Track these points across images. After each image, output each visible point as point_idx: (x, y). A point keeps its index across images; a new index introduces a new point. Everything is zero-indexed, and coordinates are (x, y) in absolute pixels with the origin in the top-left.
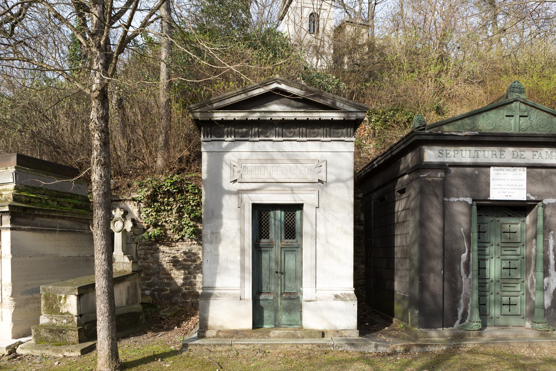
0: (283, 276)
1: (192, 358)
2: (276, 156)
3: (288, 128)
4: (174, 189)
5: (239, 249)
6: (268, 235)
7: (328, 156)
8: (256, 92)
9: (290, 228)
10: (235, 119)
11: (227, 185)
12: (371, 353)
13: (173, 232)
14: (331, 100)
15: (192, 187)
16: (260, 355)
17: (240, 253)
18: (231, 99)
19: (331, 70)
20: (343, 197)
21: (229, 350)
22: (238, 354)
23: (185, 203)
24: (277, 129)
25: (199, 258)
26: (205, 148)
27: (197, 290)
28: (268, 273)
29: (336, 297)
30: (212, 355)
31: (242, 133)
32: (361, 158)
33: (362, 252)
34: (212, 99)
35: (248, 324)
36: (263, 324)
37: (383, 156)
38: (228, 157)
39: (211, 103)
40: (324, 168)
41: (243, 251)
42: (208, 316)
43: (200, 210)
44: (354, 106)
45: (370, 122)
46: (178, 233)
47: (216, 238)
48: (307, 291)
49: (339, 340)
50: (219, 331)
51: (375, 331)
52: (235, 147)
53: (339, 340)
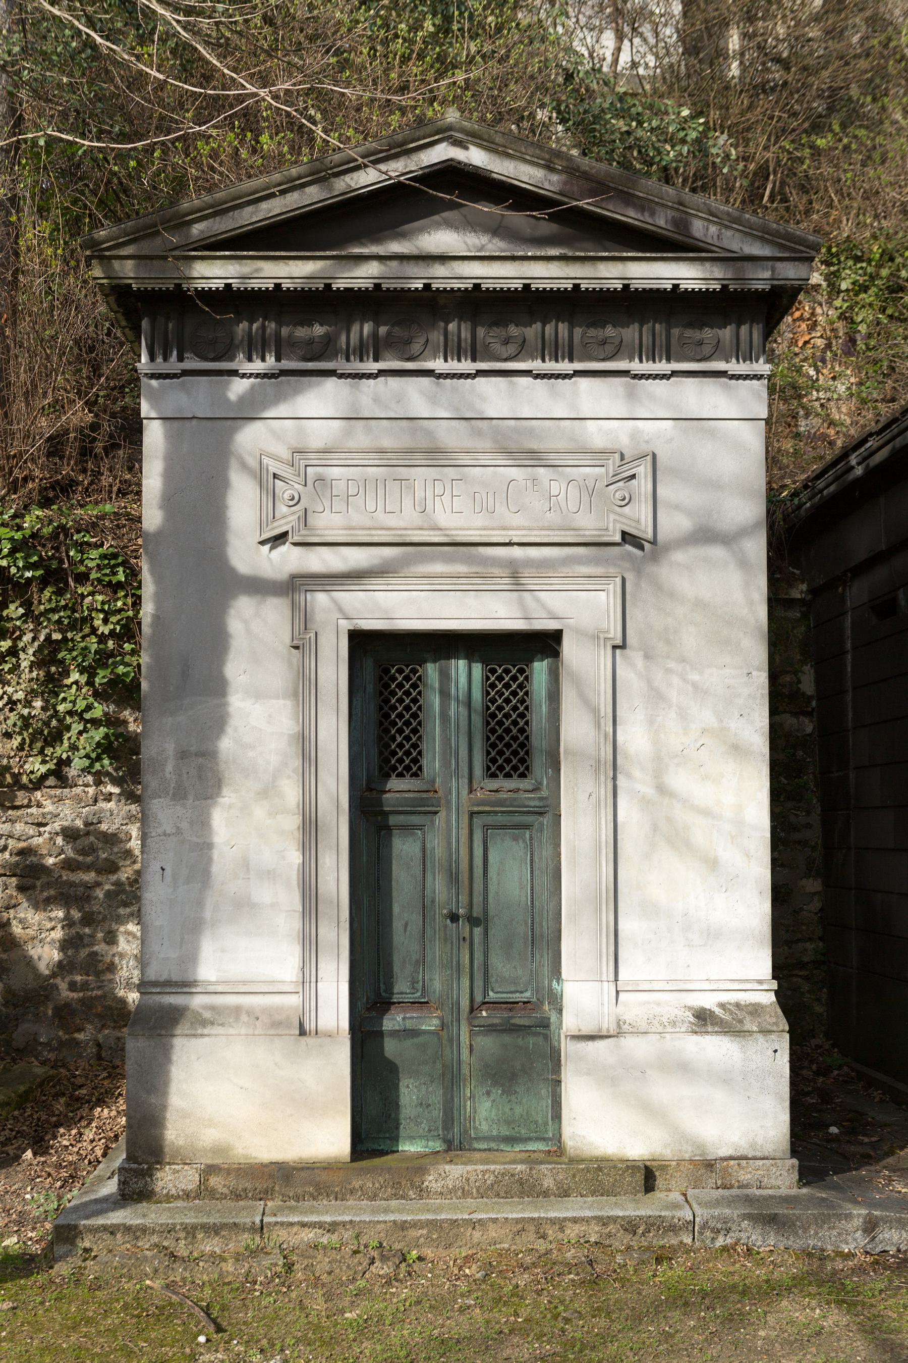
0: (478, 931)
1: (96, 1286)
2: (450, 435)
3: (496, 324)
4: (27, 567)
5: (297, 821)
6: (415, 761)
7: (658, 433)
8: (367, 178)
9: (508, 731)
10: (278, 286)
11: (246, 554)
12: (850, 1255)
13: (21, 748)
14: (670, 214)
15: (103, 557)
16: (382, 1269)
17: (298, 835)
18: (264, 205)
19: (672, 82)
20: (724, 601)
21: (255, 1253)
22: (289, 1267)
23: (72, 626)
24: (452, 326)
25: (129, 853)
26: (155, 402)
27: (121, 993)
28: (416, 919)
29: (703, 1019)
30: (179, 1273)
31: (310, 342)
32: (797, 435)
33: (808, 826)
34: (185, 205)
35: (332, 1138)
36: (396, 1139)
37: (887, 435)
38: (251, 438)
39: (181, 223)
40: (643, 484)
41: (310, 829)
42: (164, 1107)
43: (134, 652)
44: (765, 235)
45: (834, 291)
46: (41, 752)
47: (202, 776)
48: (581, 997)
49: (717, 1203)
50: (211, 1170)
51: (867, 1159)
52: (278, 399)
53: (717, 1203)
